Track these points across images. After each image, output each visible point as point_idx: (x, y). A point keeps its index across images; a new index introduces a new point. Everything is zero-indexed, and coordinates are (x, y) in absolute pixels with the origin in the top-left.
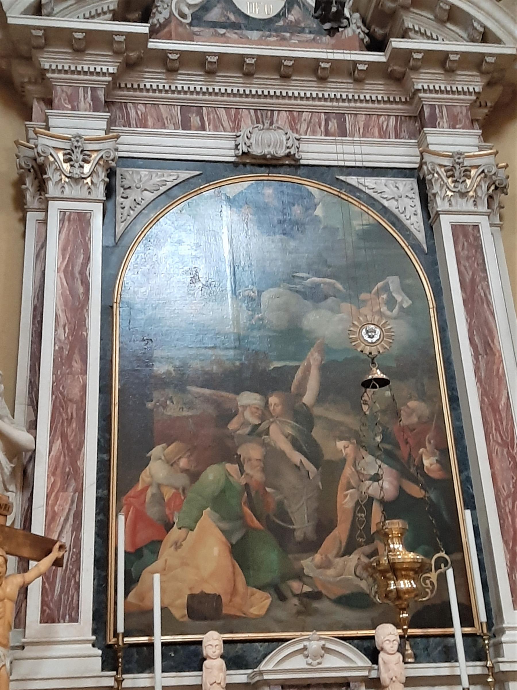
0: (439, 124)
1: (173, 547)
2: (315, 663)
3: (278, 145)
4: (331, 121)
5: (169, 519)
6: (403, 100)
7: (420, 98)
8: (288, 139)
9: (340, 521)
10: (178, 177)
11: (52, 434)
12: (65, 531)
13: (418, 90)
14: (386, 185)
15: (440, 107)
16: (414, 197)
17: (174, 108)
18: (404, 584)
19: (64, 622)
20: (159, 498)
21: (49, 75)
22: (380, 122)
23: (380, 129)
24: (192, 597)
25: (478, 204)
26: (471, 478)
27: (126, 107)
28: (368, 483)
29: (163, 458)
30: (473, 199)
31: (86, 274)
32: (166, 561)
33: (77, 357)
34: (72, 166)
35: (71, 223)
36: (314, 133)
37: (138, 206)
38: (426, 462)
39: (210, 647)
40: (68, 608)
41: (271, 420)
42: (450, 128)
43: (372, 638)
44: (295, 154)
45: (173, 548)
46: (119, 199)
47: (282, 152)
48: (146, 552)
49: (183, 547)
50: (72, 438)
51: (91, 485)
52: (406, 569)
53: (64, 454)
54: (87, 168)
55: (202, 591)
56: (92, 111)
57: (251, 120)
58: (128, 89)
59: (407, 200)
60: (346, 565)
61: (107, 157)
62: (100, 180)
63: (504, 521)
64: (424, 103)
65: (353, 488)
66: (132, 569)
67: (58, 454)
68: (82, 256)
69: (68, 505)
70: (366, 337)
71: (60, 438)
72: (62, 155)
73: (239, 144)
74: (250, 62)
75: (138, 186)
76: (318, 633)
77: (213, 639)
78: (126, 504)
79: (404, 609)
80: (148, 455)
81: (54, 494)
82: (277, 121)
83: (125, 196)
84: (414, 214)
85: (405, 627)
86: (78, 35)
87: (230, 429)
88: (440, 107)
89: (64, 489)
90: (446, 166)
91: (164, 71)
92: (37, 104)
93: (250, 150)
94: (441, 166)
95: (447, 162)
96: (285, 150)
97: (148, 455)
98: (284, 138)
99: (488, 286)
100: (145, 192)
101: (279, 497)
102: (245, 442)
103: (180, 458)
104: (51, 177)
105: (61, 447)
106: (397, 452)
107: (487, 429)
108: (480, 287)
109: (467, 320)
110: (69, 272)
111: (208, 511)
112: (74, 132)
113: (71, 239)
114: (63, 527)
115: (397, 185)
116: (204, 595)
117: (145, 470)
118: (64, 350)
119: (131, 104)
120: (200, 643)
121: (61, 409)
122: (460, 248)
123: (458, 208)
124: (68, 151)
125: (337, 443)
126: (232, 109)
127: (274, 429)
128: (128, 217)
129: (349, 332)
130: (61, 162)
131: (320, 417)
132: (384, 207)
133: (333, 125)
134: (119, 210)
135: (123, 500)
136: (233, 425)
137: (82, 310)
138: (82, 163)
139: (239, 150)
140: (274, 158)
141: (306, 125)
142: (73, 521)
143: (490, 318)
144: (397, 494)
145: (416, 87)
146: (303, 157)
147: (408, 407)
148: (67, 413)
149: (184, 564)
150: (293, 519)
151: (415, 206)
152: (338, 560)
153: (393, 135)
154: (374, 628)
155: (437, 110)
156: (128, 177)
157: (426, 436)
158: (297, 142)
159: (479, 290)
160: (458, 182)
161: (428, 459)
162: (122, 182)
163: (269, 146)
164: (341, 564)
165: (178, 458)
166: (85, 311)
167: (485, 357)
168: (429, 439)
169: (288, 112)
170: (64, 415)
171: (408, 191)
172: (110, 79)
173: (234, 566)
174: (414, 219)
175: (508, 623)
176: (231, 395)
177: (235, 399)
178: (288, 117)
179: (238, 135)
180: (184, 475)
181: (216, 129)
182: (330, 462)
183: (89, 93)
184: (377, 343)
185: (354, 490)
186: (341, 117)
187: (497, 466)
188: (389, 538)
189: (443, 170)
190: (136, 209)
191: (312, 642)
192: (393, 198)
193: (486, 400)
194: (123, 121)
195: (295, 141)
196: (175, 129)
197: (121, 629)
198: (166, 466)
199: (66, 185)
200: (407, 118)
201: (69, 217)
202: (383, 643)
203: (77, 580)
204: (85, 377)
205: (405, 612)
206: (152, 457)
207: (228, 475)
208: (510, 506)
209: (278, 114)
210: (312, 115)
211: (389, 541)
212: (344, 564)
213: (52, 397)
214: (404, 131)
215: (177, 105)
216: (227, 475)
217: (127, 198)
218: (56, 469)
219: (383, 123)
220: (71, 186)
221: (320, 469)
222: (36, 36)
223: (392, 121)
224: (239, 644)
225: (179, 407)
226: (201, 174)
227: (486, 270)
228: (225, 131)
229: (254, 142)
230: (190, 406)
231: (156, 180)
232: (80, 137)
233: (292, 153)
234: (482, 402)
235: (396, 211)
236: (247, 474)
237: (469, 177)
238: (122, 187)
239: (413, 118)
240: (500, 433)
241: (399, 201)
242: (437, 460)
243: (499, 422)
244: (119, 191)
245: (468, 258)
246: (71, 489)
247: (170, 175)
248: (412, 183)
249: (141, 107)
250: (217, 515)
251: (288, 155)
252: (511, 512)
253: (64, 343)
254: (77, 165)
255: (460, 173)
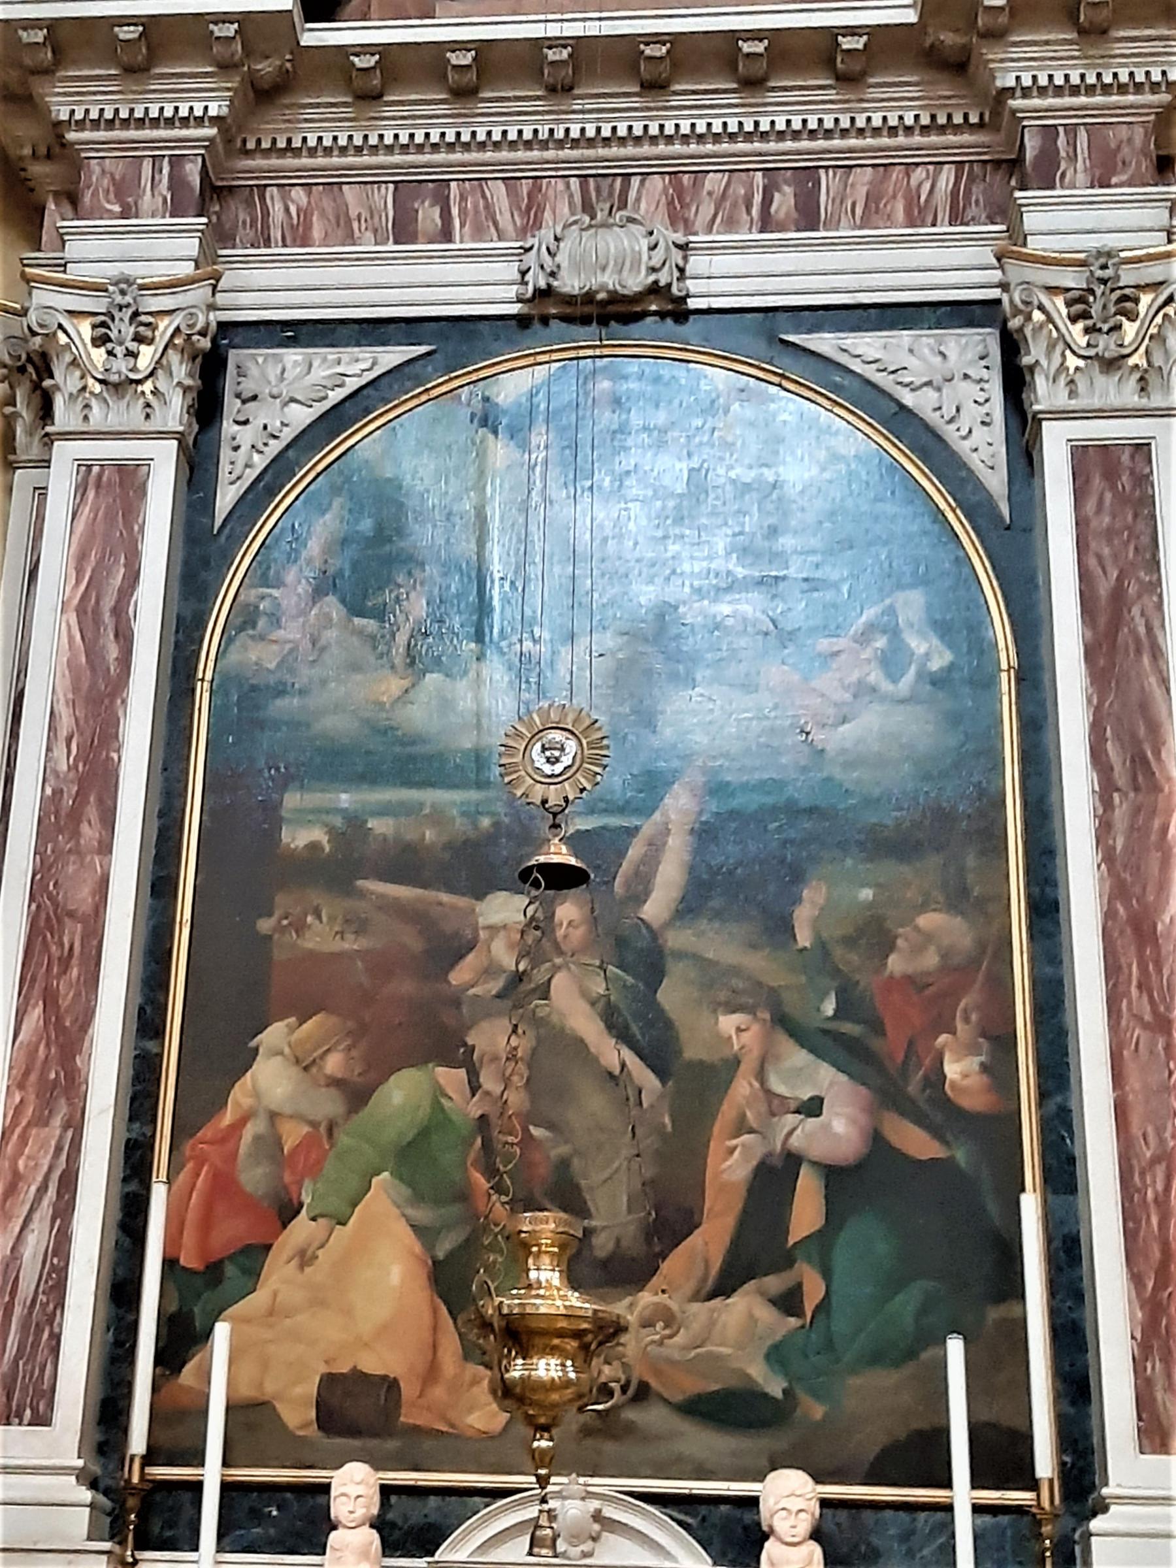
0: (1063, 175)
1: (293, 1263)
2: (575, 1551)
3: (628, 264)
4: (779, 191)
5: (291, 1200)
6: (974, 119)
7: (1014, 112)
8: (653, 248)
9: (710, 1210)
10: (374, 364)
11: (23, 992)
12: (37, 1216)
13: (1009, 92)
14: (911, 351)
15: (1071, 130)
16: (986, 378)
17: (379, 189)
18: (547, 1368)
19: (20, 1424)
20: (271, 1145)
21: (72, 136)
22: (914, 182)
23: (912, 199)
24: (329, 1381)
25: (1149, 389)
26: (1071, 1111)
27: (262, 198)
28: (791, 1119)
29: (287, 1050)
30: (1137, 375)
31: (127, 613)
32: (275, 1294)
33: (92, 812)
34: (110, 353)
35: (103, 491)
36: (731, 224)
37: (272, 442)
38: (952, 1070)
39: (343, 1499)
40: (31, 1393)
41: (558, 961)
42: (1092, 187)
43: (752, 1502)
44: (669, 285)
45: (294, 1263)
46: (228, 427)
47: (636, 282)
48: (230, 1270)
49: (317, 1262)
50: (67, 1003)
51: (102, 1112)
52: (561, 1333)
53: (48, 1037)
54: (147, 355)
55: (355, 1367)
56: (168, 215)
57: (570, 203)
58: (267, 153)
59: (965, 385)
60: (716, 1320)
61: (190, 326)
62: (176, 381)
63: (1138, 1222)
64: (1025, 123)
65: (751, 1131)
66: (196, 1310)
67: (34, 1039)
68: (122, 571)
69: (49, 1157)
70: (540, 762)
71: (41, 1003)
72: (89, 328)
73: (529, 268)
74: (557, 58)
75: (275, 391)
76: (582, 1480)
77: (352, 1481)
78: (191, 1158)
79: (545, 1428)
80: (253, 1044)
81: (18, 1131)
82: (638, 200)
83: (242, 419)
84: (983, 423)
85: (542, 1472)
86: (126, 32)
87: (454, 983)
88: (1071, 130)
89: (40, 1120)
90: (1068, 290)
91: (349, 99)
92: (53, 207)
93: (555, 283)
94: (1052, 290)
95: (1071, 279)
96: (647, 275)
97: (253, 1044)
98: (644, 243)
99: (1159, 606)
100: (293, 405)
101: (564, 1150)
102: (488, 1015)
103: (328, 1050)
104: (61, 385)
105: (41, 1022)
106: (876, 1044)
107: (1115, 985)
108: (1136, 611)
109: (1089, 701)
110: (89, 610)
111: (384, 1180)
112: (113, 270)
113: (100, 527)
114: (32, 1210)
115: (942, 348)
116: (358, 1377)
117: (243, 1079)
118: (65, 795)
119: (275, 189)
120: (325, 1489)
121: (49, 935)
122: (1090, 506)
123: (1097, 403)
124: (102, 318)
125: (721, 1018)
126: (524, 181)
127: (560, 983)
128: (248, 470)
129: (503, 749)
130: (85, 345)
131: (680, 955)
132: (902, 407)
133: (784, 201)
134: (225, 454)
135: (187, 1148)
136: (459, 976)
137: (112, 702)
138: (133, 346)
139: (527, 284)
140: (615, 298)
141: (713, 206)
142: (58, 1192)
143: (1158, 692)
144: (865, 1151)
145: (999, 83)
146: (692, 290)
147: (917, 929)
148: (62, 945)
149: (318, 1302)
150: (590, 1203)
151: (987, 401)
152: (696, 1307)
153: (944, 214)
154: (762, 1481)
155: (1061, 141)
156: (254, 371)
157: (960, 1000)
158: (677, 256)
159: (1133, 619)
160: (1100, 330)
161: (958, 1061)
162: (239, 383)
163: (604, 269)
164: (703, 1318)
165: (320, 1051)
166: (119, 701)
167: (1132, 795)
168: (965, 1011)
169: (667, 178)
170: (54, 948)
171: (971, 363)
172: (213, 131)
173: (435, 1311)
174: (981, 435)
175: (1119, 1485)
176: (462, 902)
177: (473, 910)
178: (665, 189)
179: (528, 245)
180: (333, 1091)
181: (479, 233)
182: (701, 1067)
183: (166, 170)
184: (565, 777)
185: (752, 1136)
186: (806, 179)
187: (1134, 1082)
188: (531, 1253)
189: (1060, 301)
190: (265, 449)
191: (569, 1501)
192: (929, 383)
193: (1121, 910)
194: (252, 234)
195: (674, 250)
196: (376, 244)
197: (138, 1443)
198: (295, 1071)
199: (94, 403)
200: (989, 167)
201: (100, 476)
202: (772, 1516)
203: (56, 1330)
204: (106, 859)
205: (546, 1435)
206: (261, 1050)
207: (439, 1092)
208: (1160, 1187)
209: (642, 182)
210: (730, 177)
211: (530, 1261)
212: (711, 1317)
213: (29, 906)
214: (977, 202)
215: (386, 182)
216: (438, 1093)
217: (246, 422)
218: (27, 1073)
219: (920, 185)
220: (105, 400)
221: (670, 1083)
222: (29, 44)
223: (947, 177)
224: (432, 1498)
225: (337, 929)
226: (429, 354)
227: (1158, 563)
228: (500, 238)
229: (565, 265)
230: (360, 926)
231: (320, 373)
232: (129, 281)
233: (662, 283)
234: (1109, 915)
235: (933, 418)
236: (487, 1093)
237: (1132, 317)
238: (238, 396)
239: (1004, 166)
240: (1151, 997)
241: (944, 391)
242: (982, 1064)
243: (1151, 967)
244: (231, 405)
245: (1110, 534)
246: (57, 1121)
247: (357, 360)
248: (984, 340)
249: (298, 194)
250: (406, 1191)
251: (655, 290)
252: (1162, 1201)
253: (65, 780)
254: (120, 351)
255: (1104, 307)
